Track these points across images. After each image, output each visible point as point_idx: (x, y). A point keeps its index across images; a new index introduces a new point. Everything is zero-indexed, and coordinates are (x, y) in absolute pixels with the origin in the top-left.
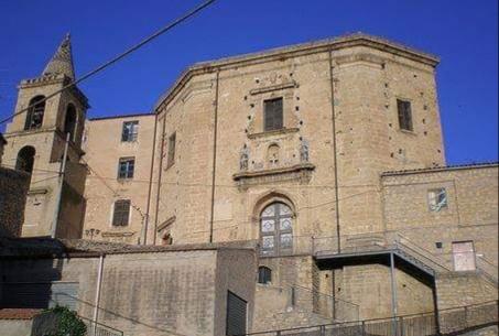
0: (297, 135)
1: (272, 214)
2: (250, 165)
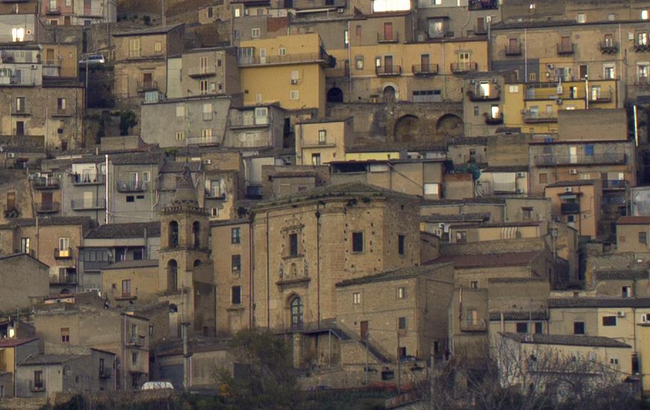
0: (303, 259)
1: (296, 304)
2: (284, 276)
